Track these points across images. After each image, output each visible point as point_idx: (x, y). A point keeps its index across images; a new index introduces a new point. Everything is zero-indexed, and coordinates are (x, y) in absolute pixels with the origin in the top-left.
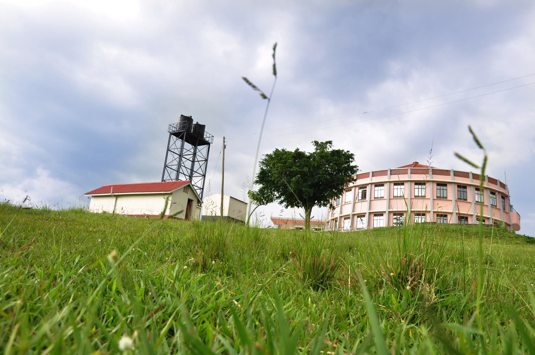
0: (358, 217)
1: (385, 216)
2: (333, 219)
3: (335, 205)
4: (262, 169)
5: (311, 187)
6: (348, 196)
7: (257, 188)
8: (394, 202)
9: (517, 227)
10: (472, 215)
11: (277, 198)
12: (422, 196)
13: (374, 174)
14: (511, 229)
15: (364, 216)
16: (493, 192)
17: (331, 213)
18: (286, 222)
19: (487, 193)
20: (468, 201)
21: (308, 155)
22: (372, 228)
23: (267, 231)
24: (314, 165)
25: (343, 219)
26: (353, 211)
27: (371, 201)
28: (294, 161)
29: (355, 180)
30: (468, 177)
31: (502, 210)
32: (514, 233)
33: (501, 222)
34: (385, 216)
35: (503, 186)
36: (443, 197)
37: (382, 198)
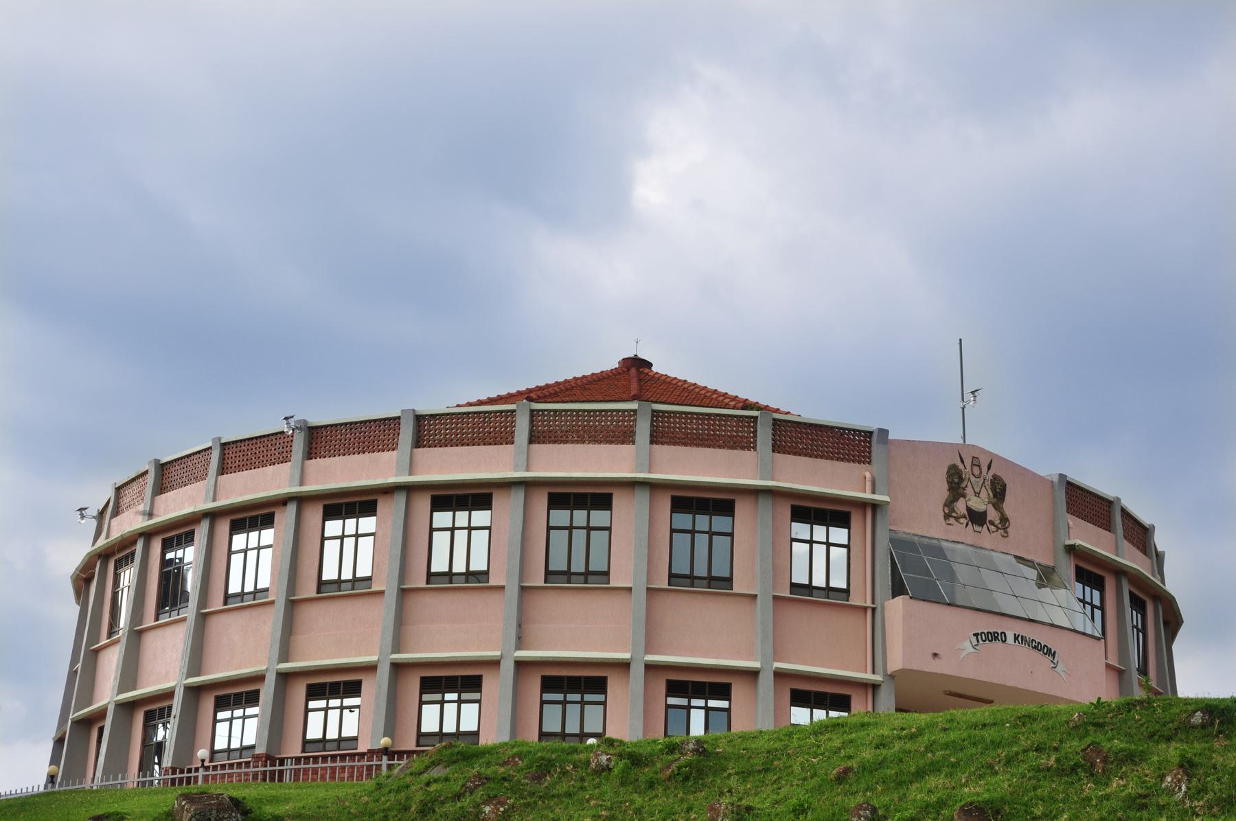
1: (375, 688)
12: (469, 575)
25: (208, 703)
30: (1107, 526)
36: (711, 580)
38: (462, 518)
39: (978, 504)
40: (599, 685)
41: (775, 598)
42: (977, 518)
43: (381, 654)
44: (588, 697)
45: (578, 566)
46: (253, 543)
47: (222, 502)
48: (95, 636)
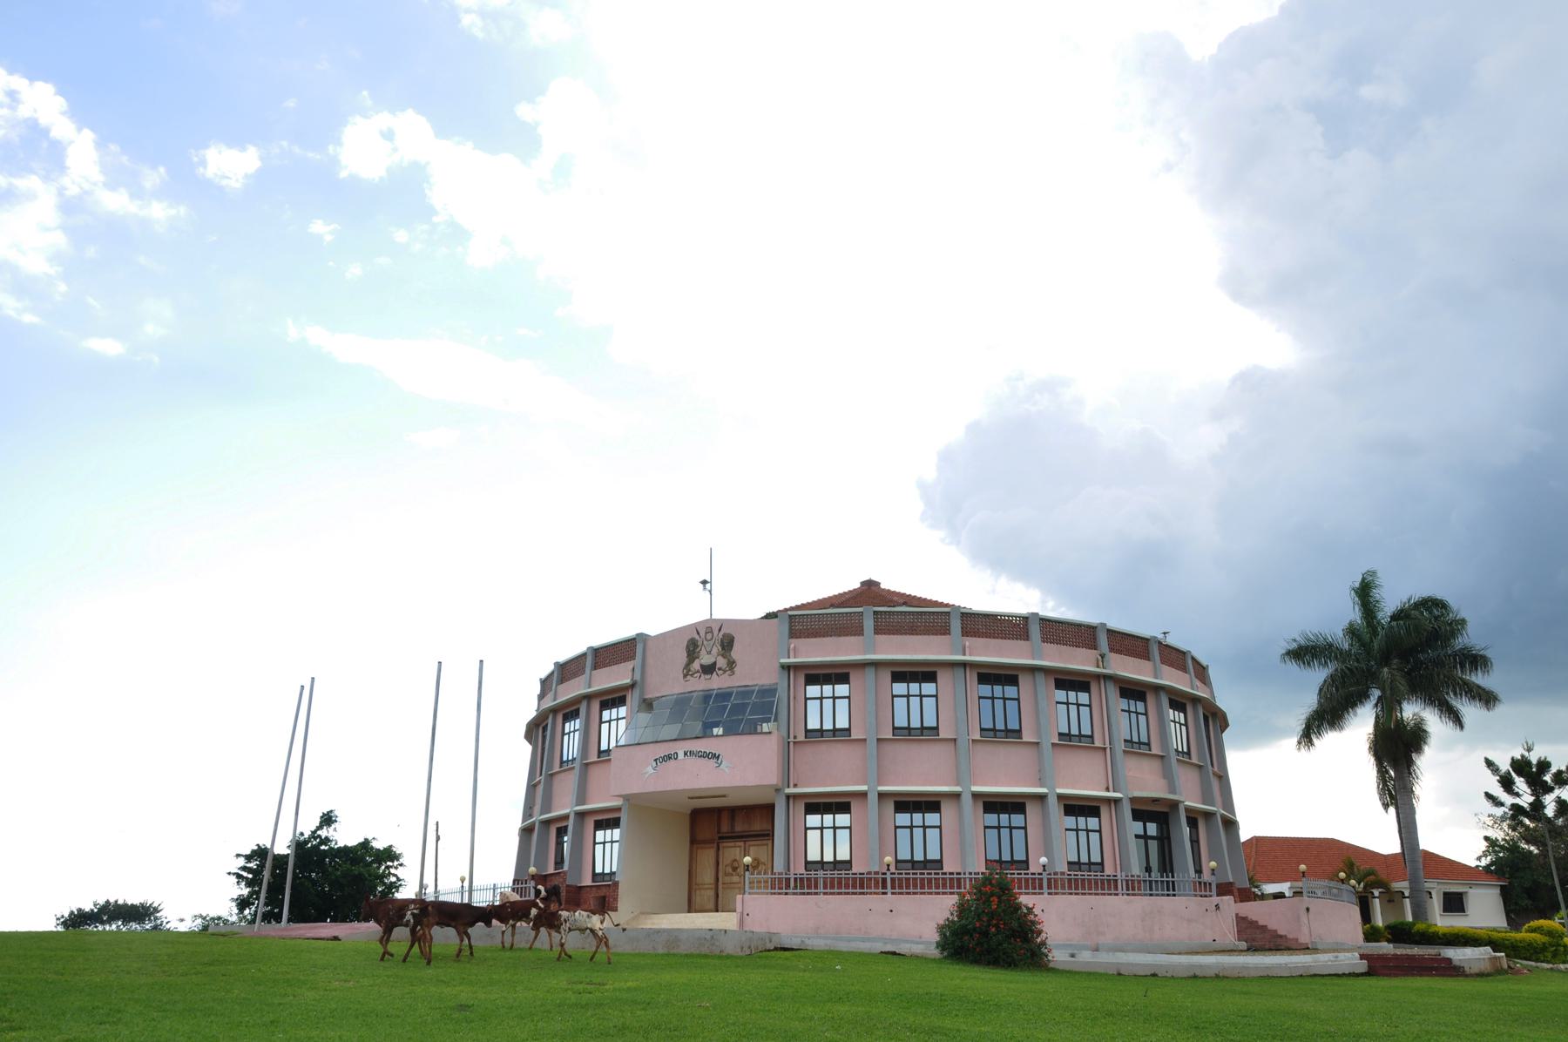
2: (547, 823)
8: (807, 757)
12: (835, 731)
25: (590, 823)
30: (944, 630)
35: (1176, 657)
36: (1008, 732)
39: (706, 659)
42: (709, 669)
45: (1000, 726)
47: (595, 688)
48: (550, 766)
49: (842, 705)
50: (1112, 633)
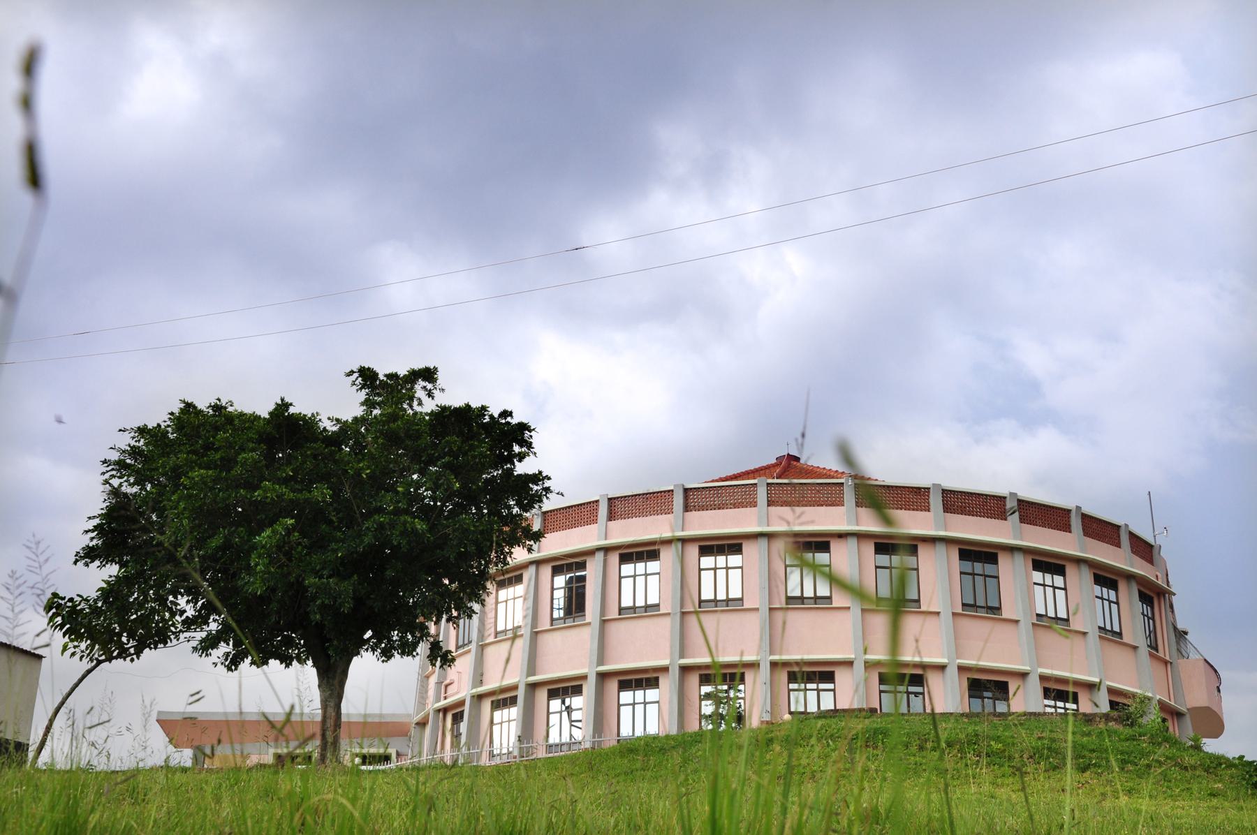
0: (553, 694)
2: (445, 710)
3: (452, 647)
4: (115, 492)
5: (343, 569)
6: (507, 606)
7: (91, 581)
9: (1212, 723)
10: (1024, 675)
11: (189, 624)
13: (618, 507)
14: (1184, 732)
15: (577, 690)
16: (1106, 578)
17: (433, 680)
18: (235, 728)
19: (1080, 580)
20: (1006, 614)
21: (332, 428)
22: (610, 741)
23: (130, 784)
24: (358, 473)
25: (486, 705)
26: (532, 668)
27: (604, 622)
28: (270, 457)
29: (537, 536)
30: (1067, 528)
31: (1144, 650)
32: (1197, 747)
33: (1145, 700)
34: (668, 684)
35: (1144, 549)
37: (650, 609)
38: (721, 560)
40: (829, 677)
41: (954, 614)
43: (672, 660)
44: (822, 686)
45: (640, 602)
46: (510, 596)
49: (735, 575)
50: (945, 492)
